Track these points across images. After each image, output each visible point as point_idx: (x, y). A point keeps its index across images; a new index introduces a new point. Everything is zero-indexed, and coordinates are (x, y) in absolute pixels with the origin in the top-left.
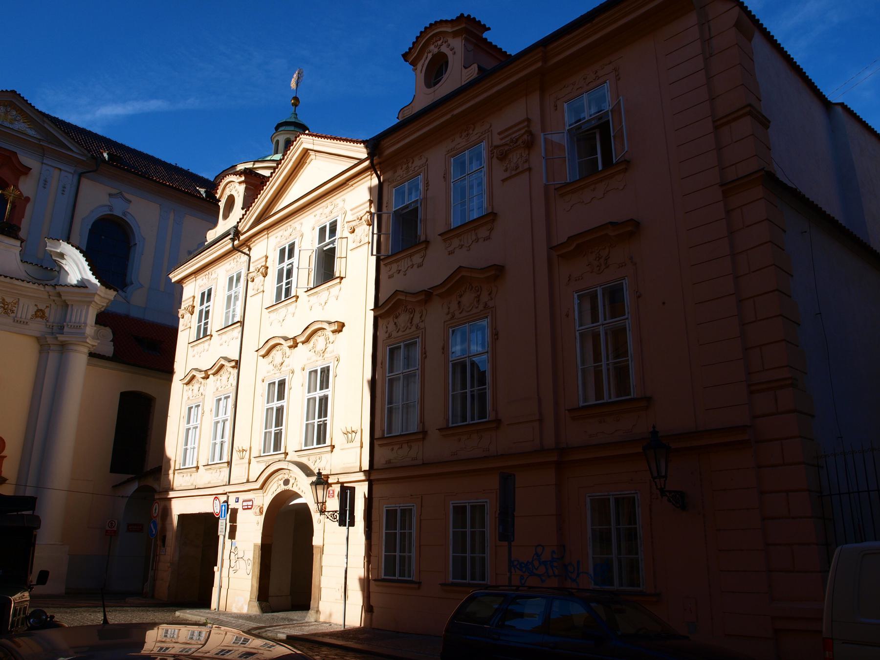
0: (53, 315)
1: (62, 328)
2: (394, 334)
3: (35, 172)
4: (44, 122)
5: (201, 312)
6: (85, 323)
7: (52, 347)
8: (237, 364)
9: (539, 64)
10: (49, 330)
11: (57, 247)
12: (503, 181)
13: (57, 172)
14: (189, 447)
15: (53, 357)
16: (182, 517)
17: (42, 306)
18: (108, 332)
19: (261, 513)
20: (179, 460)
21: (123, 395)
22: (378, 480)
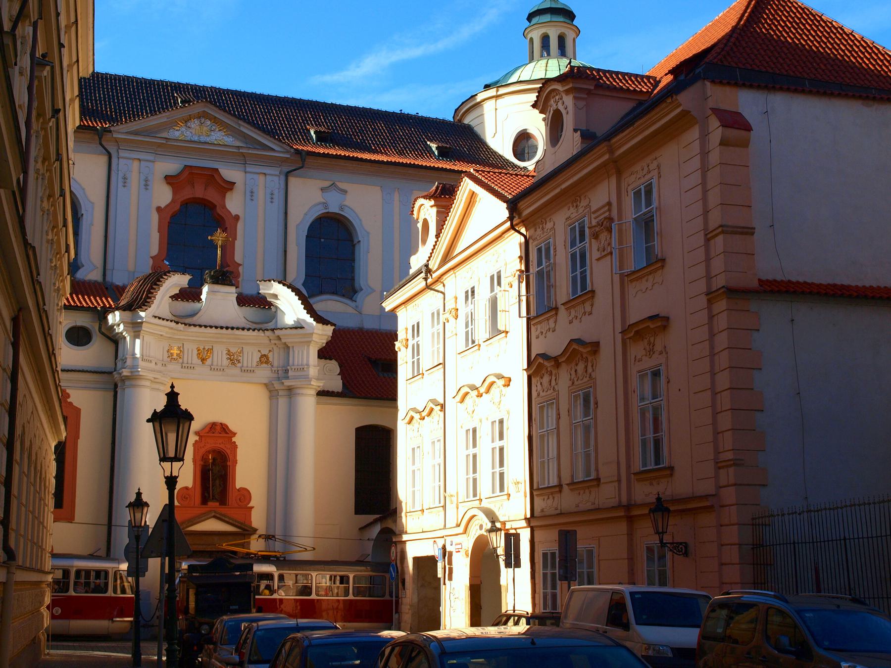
0: (276, 358)
1: (287, 371)
2: (542, 394)
3: (239, 186)
4: (239, 125)
5: (413, 346)
6: (308, 365)
7: (281, 393)
8: (443, 407)
9: (607, 157)
10: (276, 375)
11: (270, 289)
12: (598, 260)
13: (262, 177)
14: (416, 489)
15: (282, 402)
16: (416, 560)
17: (265, 352)
18: (333, 366)
19: (467, 556)
20: (410, 504)
21: (358, 430)
22: (537, 527)
